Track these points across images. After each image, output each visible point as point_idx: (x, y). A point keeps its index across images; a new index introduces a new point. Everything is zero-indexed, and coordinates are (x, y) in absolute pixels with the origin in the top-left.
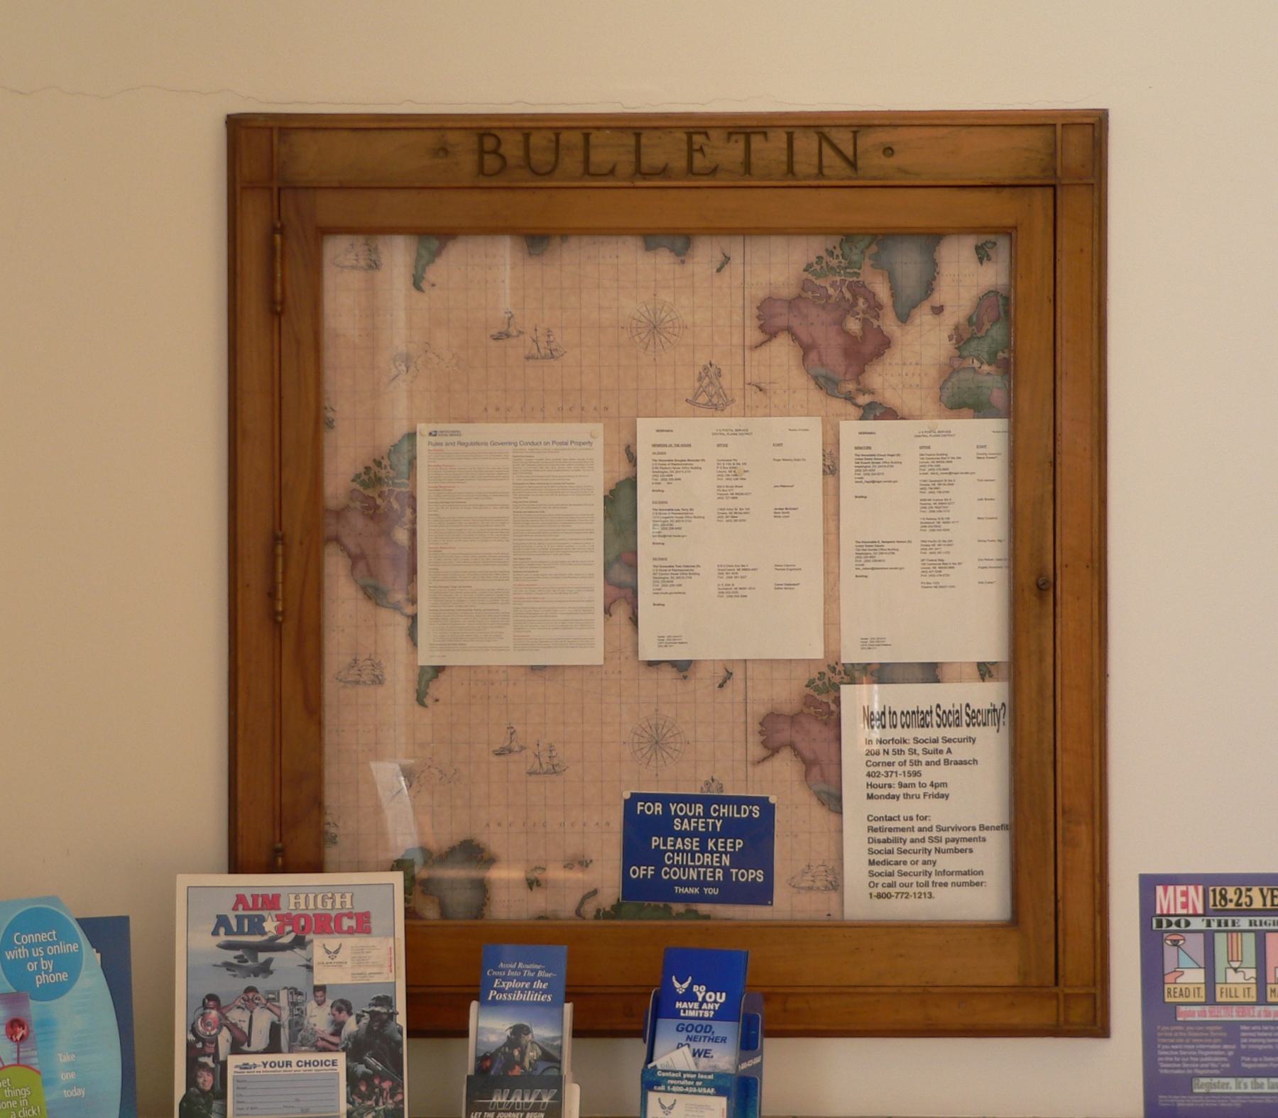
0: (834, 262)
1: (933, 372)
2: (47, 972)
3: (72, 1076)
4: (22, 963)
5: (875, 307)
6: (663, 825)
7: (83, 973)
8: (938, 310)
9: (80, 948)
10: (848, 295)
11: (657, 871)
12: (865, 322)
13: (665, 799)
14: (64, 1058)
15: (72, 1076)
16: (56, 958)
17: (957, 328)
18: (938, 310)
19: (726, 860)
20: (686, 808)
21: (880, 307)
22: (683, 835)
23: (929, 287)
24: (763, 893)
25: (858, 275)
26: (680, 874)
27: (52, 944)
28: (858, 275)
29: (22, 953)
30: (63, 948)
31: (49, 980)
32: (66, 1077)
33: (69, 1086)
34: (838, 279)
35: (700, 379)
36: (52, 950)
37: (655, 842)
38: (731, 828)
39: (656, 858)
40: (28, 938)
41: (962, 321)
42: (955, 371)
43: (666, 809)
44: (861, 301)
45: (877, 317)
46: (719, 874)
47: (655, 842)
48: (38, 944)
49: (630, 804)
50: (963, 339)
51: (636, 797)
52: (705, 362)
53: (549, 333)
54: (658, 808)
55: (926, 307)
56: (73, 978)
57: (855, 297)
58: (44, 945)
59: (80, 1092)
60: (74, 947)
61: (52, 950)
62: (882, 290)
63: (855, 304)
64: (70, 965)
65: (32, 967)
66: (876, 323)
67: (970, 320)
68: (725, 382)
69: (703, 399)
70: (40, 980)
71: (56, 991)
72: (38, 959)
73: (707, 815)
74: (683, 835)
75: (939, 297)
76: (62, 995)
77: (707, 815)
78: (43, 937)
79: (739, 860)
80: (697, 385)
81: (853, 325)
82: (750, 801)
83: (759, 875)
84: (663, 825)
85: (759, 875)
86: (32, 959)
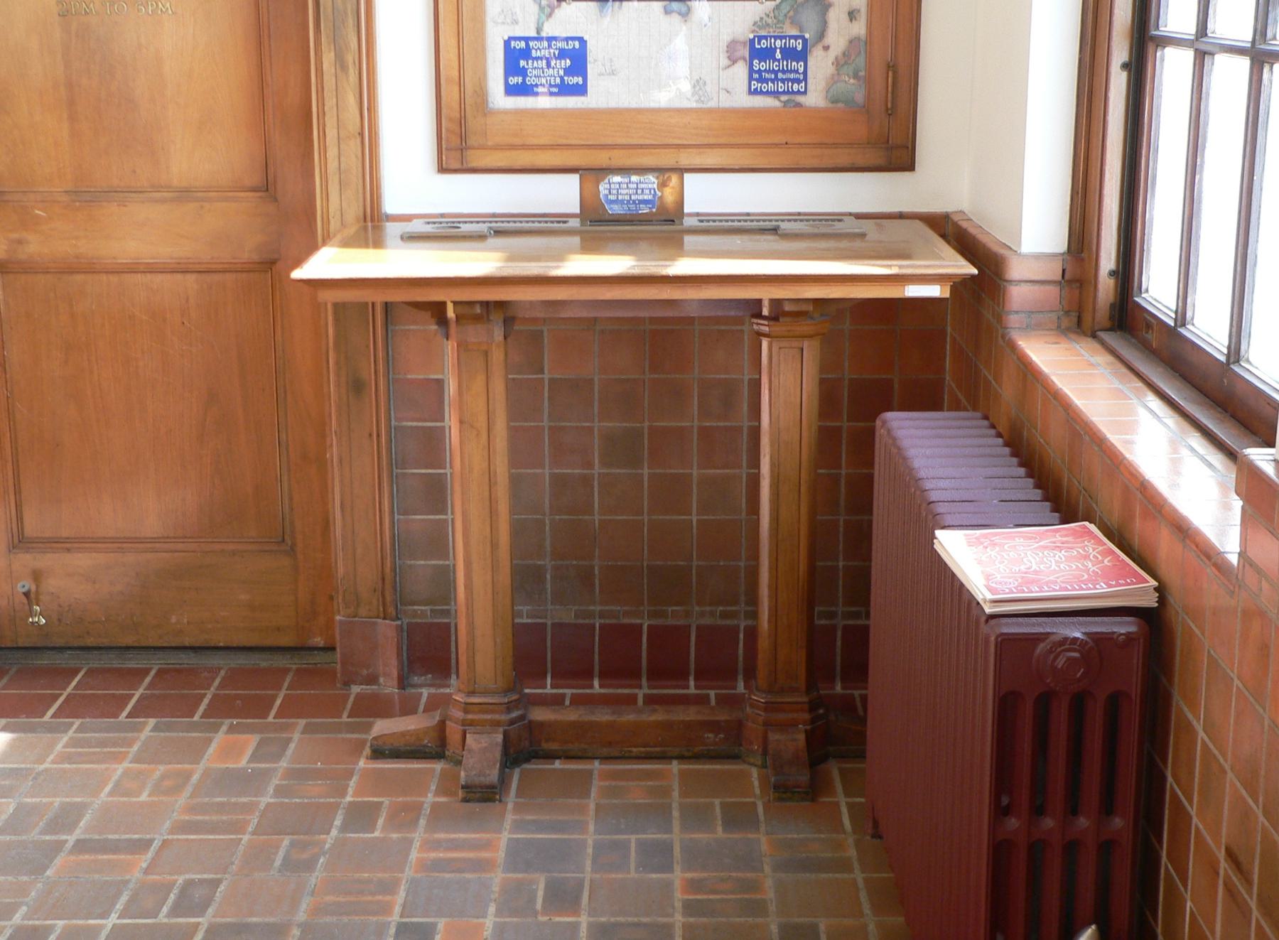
0: (769, 21)
1: (823, 84)
6: (526, 54)
8: (826, 48)
11: (524, 80)
13: (527, 39)
17: (836, 58)
18: (826, 48)
19: (562, 73)
20: (538, 44)
22: (537, 59)
23: (821, 35)
24: (581, 90)
26: (536, 81)
37: (522, 63)
38: (562, 54)
39: (523, 72)
42: (835, 82)
43: (527, 45)
46: (558, 80)
47: (522, 63)
49: (507, 43)
50: (838, 64)
51: (510, 39)
53: (611, 60)
54: (523, 44)
55: (820, 47)
67: (844, 54)
68: (708, 88)
73: (550, 46)
74: (537, 59)
75: (826, 41)
77: (550, 46)
79: (568, 72)
82: (573, 39)
83: (580, 80)
84: (526, 54)
85: (580, 80)
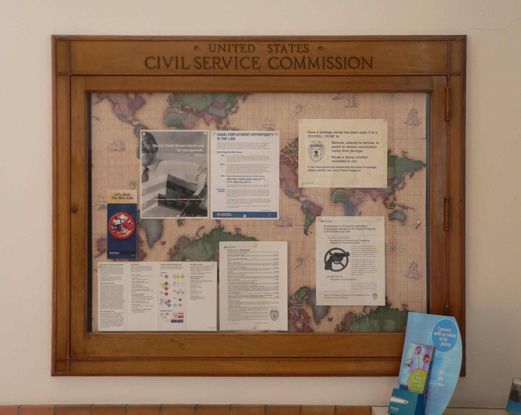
2: (445, 342)
3: (442, 379)
4: (438, 337)
5: (308, 318)
7: (456, 345)
9: (457, 337)
10: (297, 314)
12: (304, 324)
14: (441, 372)
15: (442, 379)
16: (449, 338)
21: (309, 318)
25: (301, 306)
27: (449, 333)
28: (301, 306)
29: (439, 334)
30: (452, 335)
31: (445, 345)
32: (440, 379)
33: (440, 382)
34: (294, 308)
35: (410, 268)
36: (448, 335)
40: (443, 329)
41: (339, 323)
44: (302, 316)
45: (308, 322)
48: (445, 332)
52: (411, 262)
55: (326, 318)
56: (452, 346)
57: (300, 314)
58: (446, 333)
59: (443, 385)
60: (455, 336)
61: (448, 335)
62: (310, 313)
63: (300, 317)
64: (452, 341)
65: (441, 339)
66: (307, 324)
67: (342, 323)
69: (411, 275)
70: (442, 344)
71: (446, 349)
72: (443, 337)
76: (446, 351)
78: (447, 330)
80: (409, 270)
81: (299, 325)
86: (442, 337)
